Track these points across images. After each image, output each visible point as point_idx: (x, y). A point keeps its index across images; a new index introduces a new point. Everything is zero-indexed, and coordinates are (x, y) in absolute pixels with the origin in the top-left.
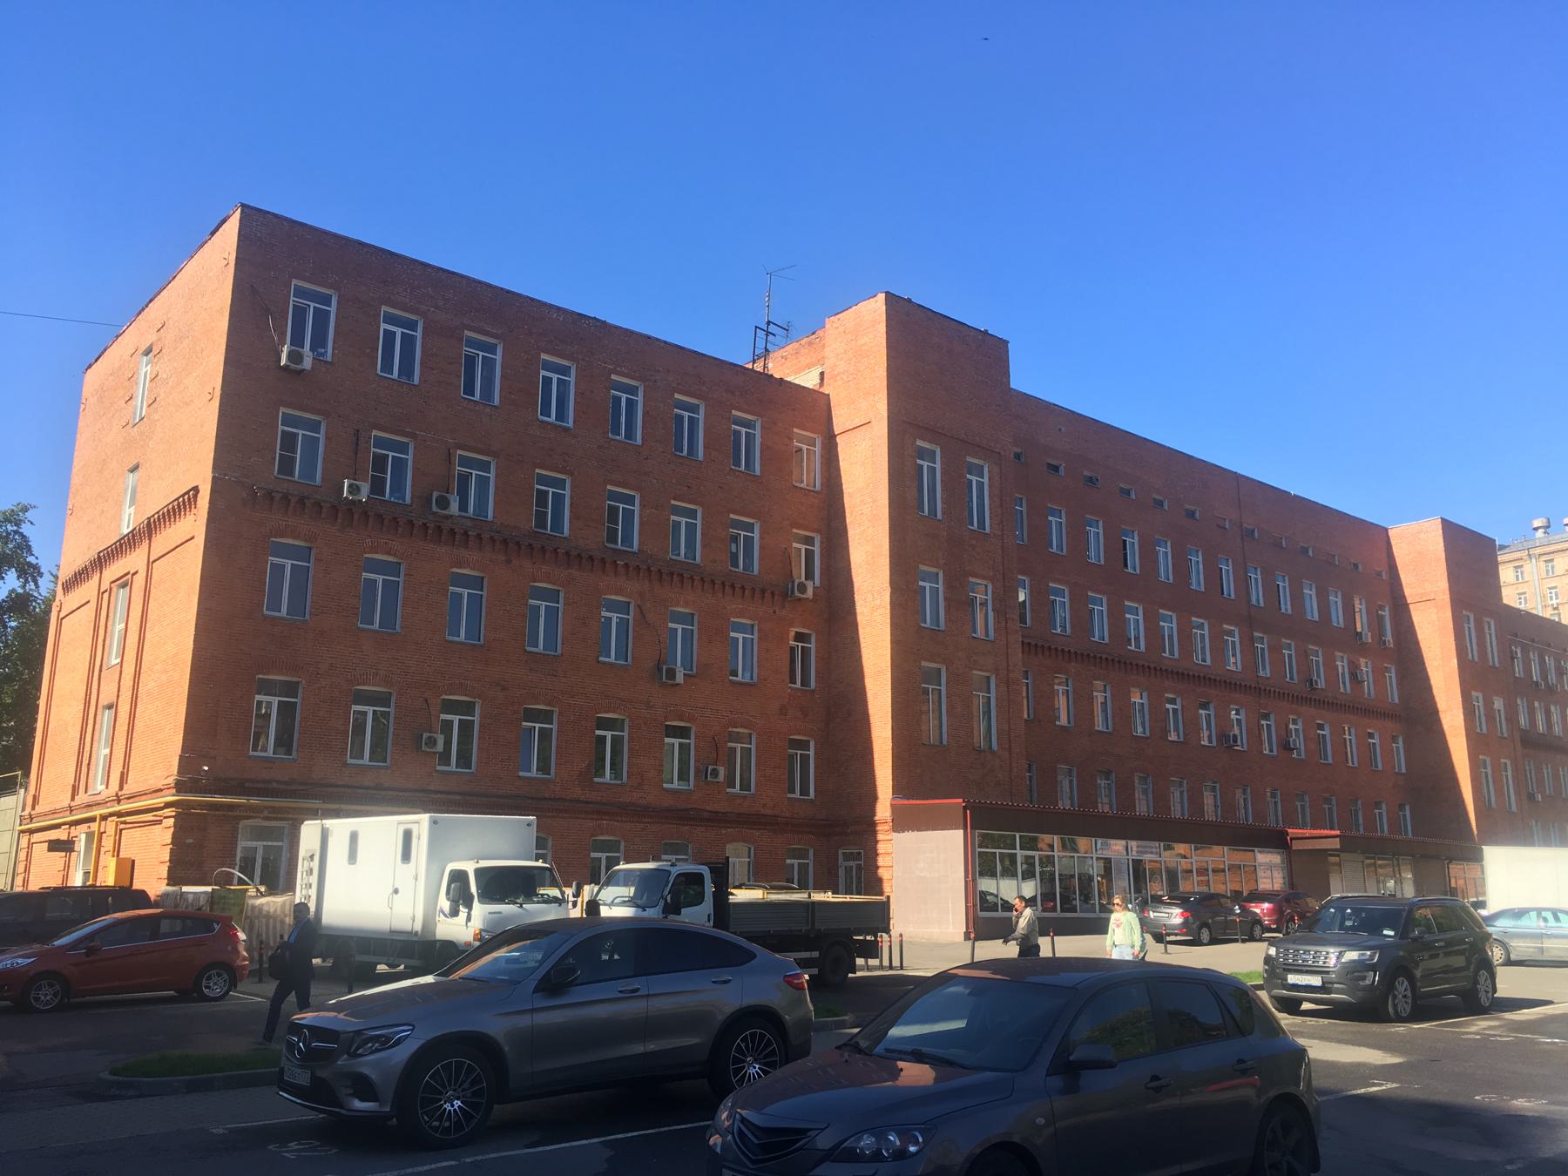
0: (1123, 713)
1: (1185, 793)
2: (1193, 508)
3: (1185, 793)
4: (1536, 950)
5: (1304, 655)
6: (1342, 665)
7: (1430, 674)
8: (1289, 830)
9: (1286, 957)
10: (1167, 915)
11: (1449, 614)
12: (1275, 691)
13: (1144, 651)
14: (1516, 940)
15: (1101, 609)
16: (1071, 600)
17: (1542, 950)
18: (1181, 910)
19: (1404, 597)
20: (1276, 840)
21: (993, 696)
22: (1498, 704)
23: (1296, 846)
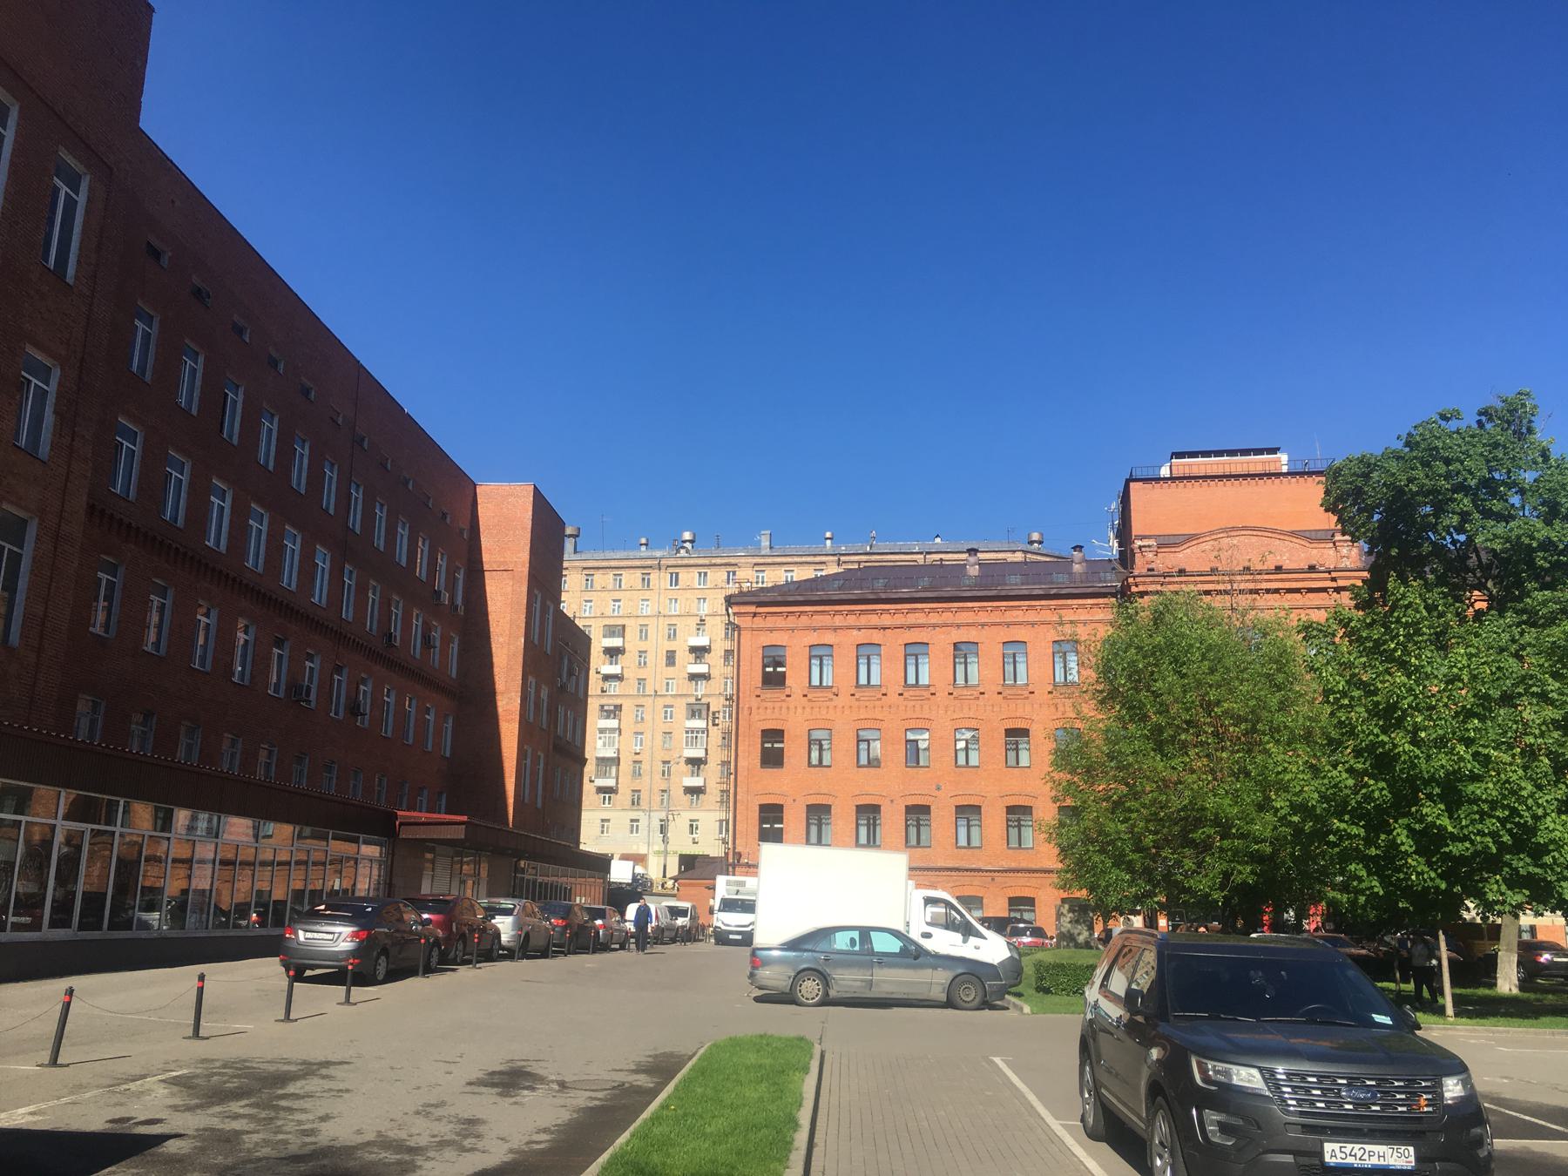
0: (183, 632)
1: (238, 755)
2: (309, 384)
3: (238, 755)
4: (864, 984)
5: (386, 604)
6: (417, 623)
7: (494, 650)
8: (399, 813)
9: (1331, 1097)
10: (330, 937)
11: (525, 589)
12: (354, 640)
13: (224, 552)
14: (839, 971)
15: (180, 477)
16: (145, 449)
17: (870, 984)
18: (355, 929)
19: (481, 562)
20: (380, 826)
21: (27, 553)
22: (544, 694)
23: (405, 833)
